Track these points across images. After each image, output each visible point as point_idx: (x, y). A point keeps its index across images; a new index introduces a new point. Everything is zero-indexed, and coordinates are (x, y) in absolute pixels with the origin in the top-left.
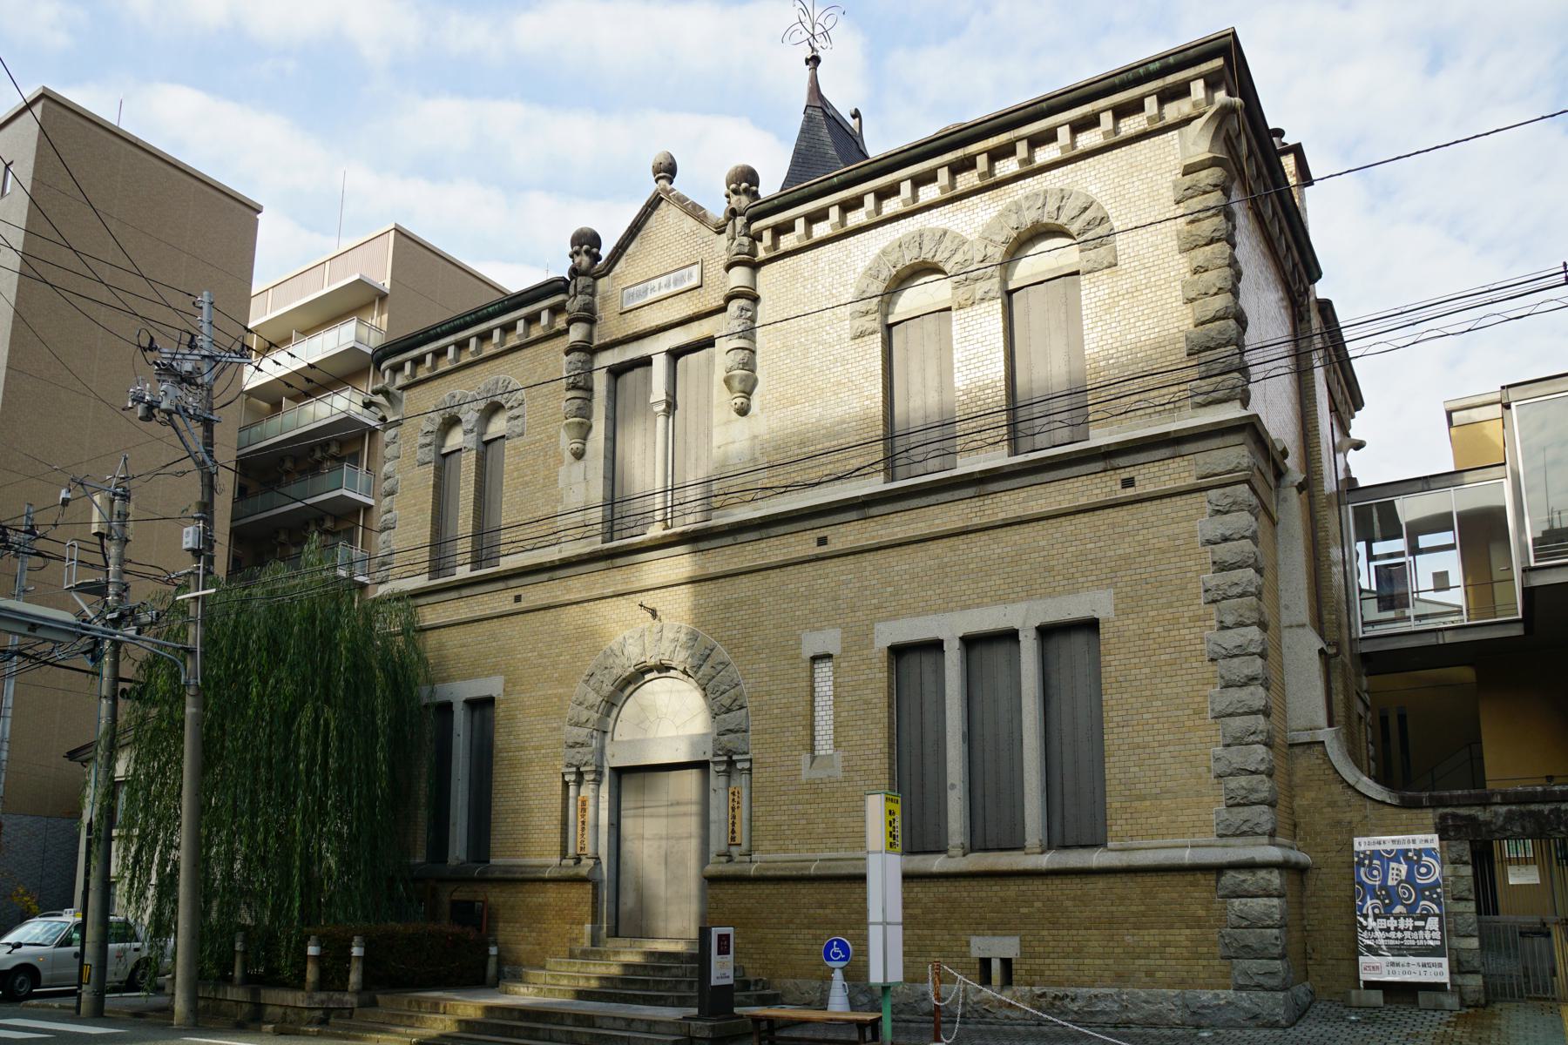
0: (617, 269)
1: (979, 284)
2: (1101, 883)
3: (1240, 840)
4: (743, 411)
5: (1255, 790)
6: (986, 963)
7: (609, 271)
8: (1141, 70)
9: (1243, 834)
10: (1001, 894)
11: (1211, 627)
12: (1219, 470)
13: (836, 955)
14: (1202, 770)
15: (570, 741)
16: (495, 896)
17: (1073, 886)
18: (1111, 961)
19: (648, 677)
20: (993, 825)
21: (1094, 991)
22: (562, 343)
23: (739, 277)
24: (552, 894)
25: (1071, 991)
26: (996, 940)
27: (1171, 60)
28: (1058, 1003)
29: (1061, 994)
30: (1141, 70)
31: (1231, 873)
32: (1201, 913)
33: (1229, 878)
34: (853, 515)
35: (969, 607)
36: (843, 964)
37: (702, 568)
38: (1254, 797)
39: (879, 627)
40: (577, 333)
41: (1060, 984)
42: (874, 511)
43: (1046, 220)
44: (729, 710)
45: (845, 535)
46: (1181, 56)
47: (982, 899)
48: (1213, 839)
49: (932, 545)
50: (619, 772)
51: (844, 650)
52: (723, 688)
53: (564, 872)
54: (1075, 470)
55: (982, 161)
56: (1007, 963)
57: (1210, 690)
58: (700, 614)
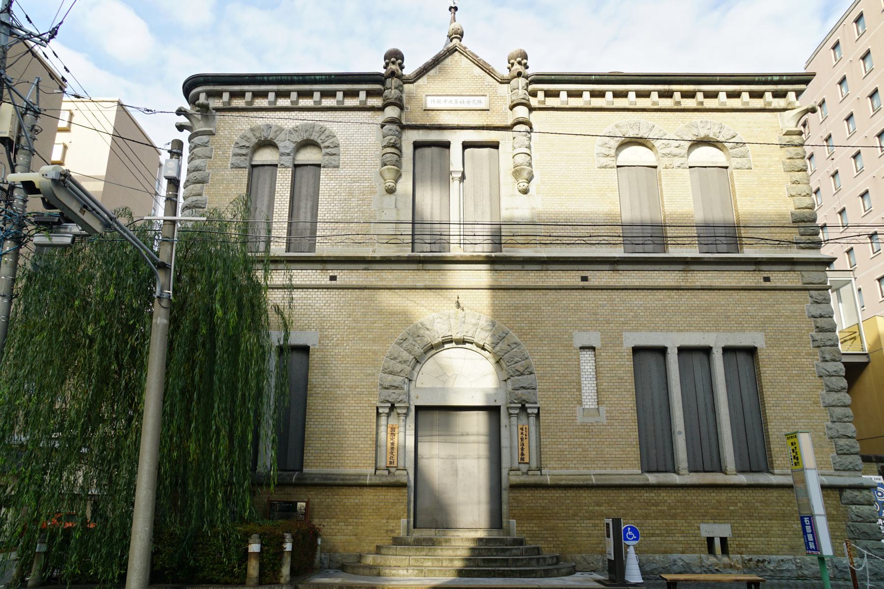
0: (420, 82)
1: (676, 158)
2: (775, 493)
3: (847, 473)
4: (525, 192)
5: (853, 447)
6: (710, 540)
7: (414, 82)
8: (769, 78)
9: (849, 470)
10: (717, 498)
11: (817, 360)
12: (815, 281)
13: (630, 536)
14: (821, 434)
15: (386, 384)
16: (318, 498)
17: (760, 494)
18: (786, 539)
19: (446, 346)
20: (706, 458)
21: (780, 557)
22: (380, 118)
23: (521, 112)
24: (369, 496)
25: (766, 557)
26: (716, 526)
27: (785, 78)
28: (760, 565)
29: (761, 559)
30: (769, 78)
31: (848, 491)
32: (835, 513)
33: (848, 494)
34: (607, 267)
35: (682, 331)
36: (635, 542)
37: (495, 280)
38: (853, 451)
39: (625, 334)
40: (392, 112)
41: (758, 553)
42: (620, 267)
43: (711, 136)
44: (522, 374)
45: (600, 277)
46: (789, 78)
47: (705, 501)
48: (832, 471)
49: (658, 293)
50: (418, 409)
51: (603, 345)
52: (517, 359)
53: (376, 481)
54: (657, 267)
55: (248, 96)
56: (723, 540)
57: (820, 391)
58: (496, 312)
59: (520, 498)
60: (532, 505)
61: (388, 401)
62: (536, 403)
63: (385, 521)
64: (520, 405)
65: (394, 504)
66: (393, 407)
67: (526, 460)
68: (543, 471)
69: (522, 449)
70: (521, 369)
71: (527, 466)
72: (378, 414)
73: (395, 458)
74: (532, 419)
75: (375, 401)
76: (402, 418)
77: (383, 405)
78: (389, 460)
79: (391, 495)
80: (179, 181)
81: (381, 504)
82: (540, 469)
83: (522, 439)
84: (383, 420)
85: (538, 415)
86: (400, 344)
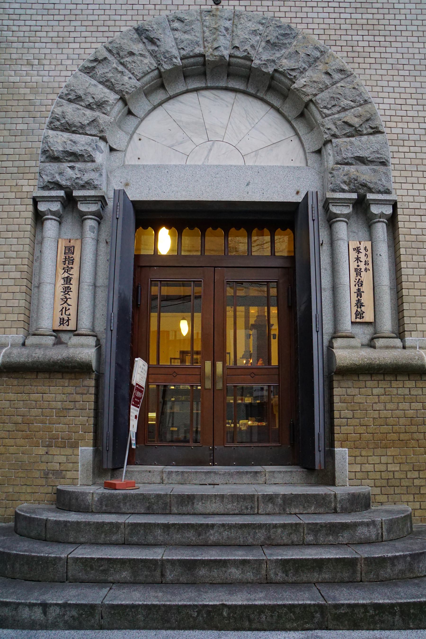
44: (358, 133)
52: (344, 103)
59: (358, 399)
60: (384, 413)
61: (59, 186)
62: (388, 192)
63: (41, 451)
64: (354, 196)
65: (63, 412)
66: (70, 202)
67: (369, 317)
68: (409, 340)
69: (359, 293)
70: (356, 122)
71: (369, 330)
72: (39, 218)
73: (72, 311)
74: (381, 230)
75: (31, 187)
76: (90, 223)
77: (46, 193)
78: (58, 315)
79: (56, 393)
80: (391, 520)
81: (34, 412)
82: (400, 333)
83: (358, 272)
84: (50, 227)
85: (392, 221)
86: (88, 70)
